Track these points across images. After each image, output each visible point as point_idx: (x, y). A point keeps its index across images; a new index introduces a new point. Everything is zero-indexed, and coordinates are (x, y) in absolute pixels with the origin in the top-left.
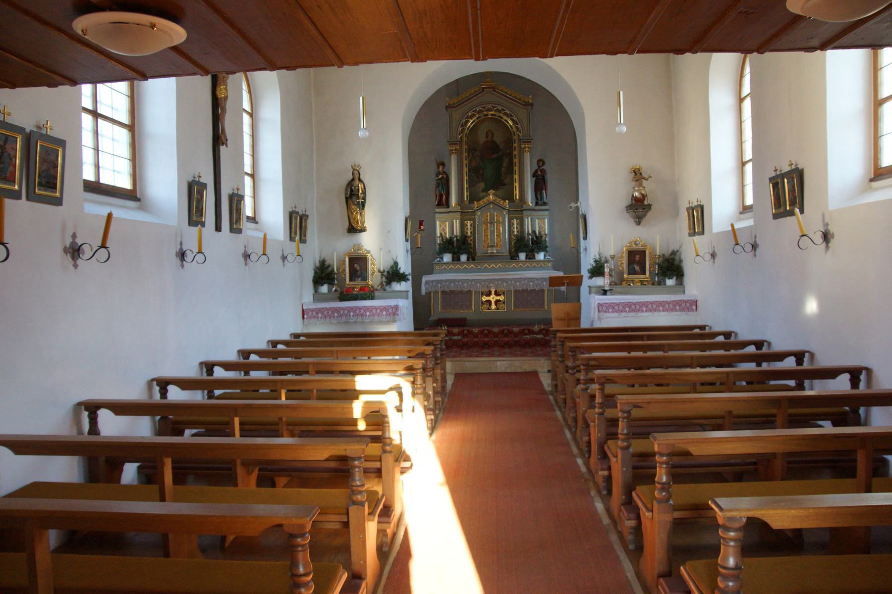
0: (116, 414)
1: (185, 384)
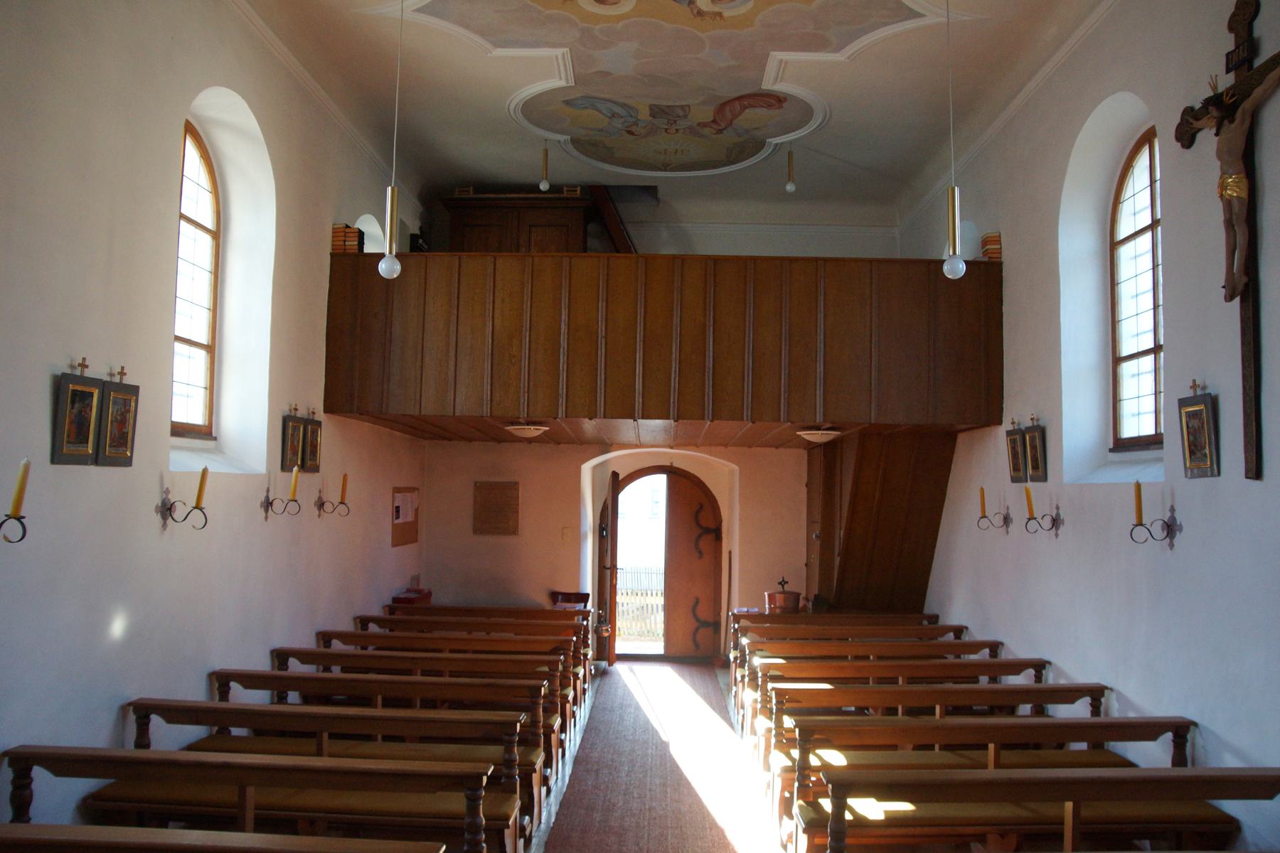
1: (251, 680)
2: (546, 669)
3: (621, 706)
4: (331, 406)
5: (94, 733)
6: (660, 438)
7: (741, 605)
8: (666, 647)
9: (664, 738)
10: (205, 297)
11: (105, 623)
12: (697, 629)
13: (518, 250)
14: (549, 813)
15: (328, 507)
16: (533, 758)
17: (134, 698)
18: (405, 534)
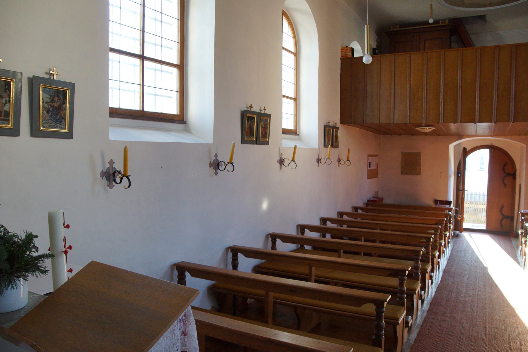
0: (283, 242)
1: (313, 229)
2: (433, 232)
3: (465, 250)
4: (343, 121)
5: (213, 259)
6: (487, 132)
7: (525, 209)
8: (487, 227)
9: (485, 265)
10: (292, 79)
11: (260, 203)
12: (502, 219)
13: (420, 51)
14: (432, 291)
15: (342, 162)
16: (426, 267)
17: (271, 232)
18: (373, 174)
